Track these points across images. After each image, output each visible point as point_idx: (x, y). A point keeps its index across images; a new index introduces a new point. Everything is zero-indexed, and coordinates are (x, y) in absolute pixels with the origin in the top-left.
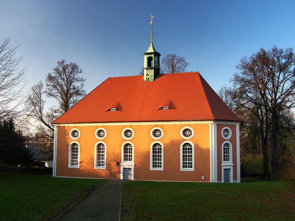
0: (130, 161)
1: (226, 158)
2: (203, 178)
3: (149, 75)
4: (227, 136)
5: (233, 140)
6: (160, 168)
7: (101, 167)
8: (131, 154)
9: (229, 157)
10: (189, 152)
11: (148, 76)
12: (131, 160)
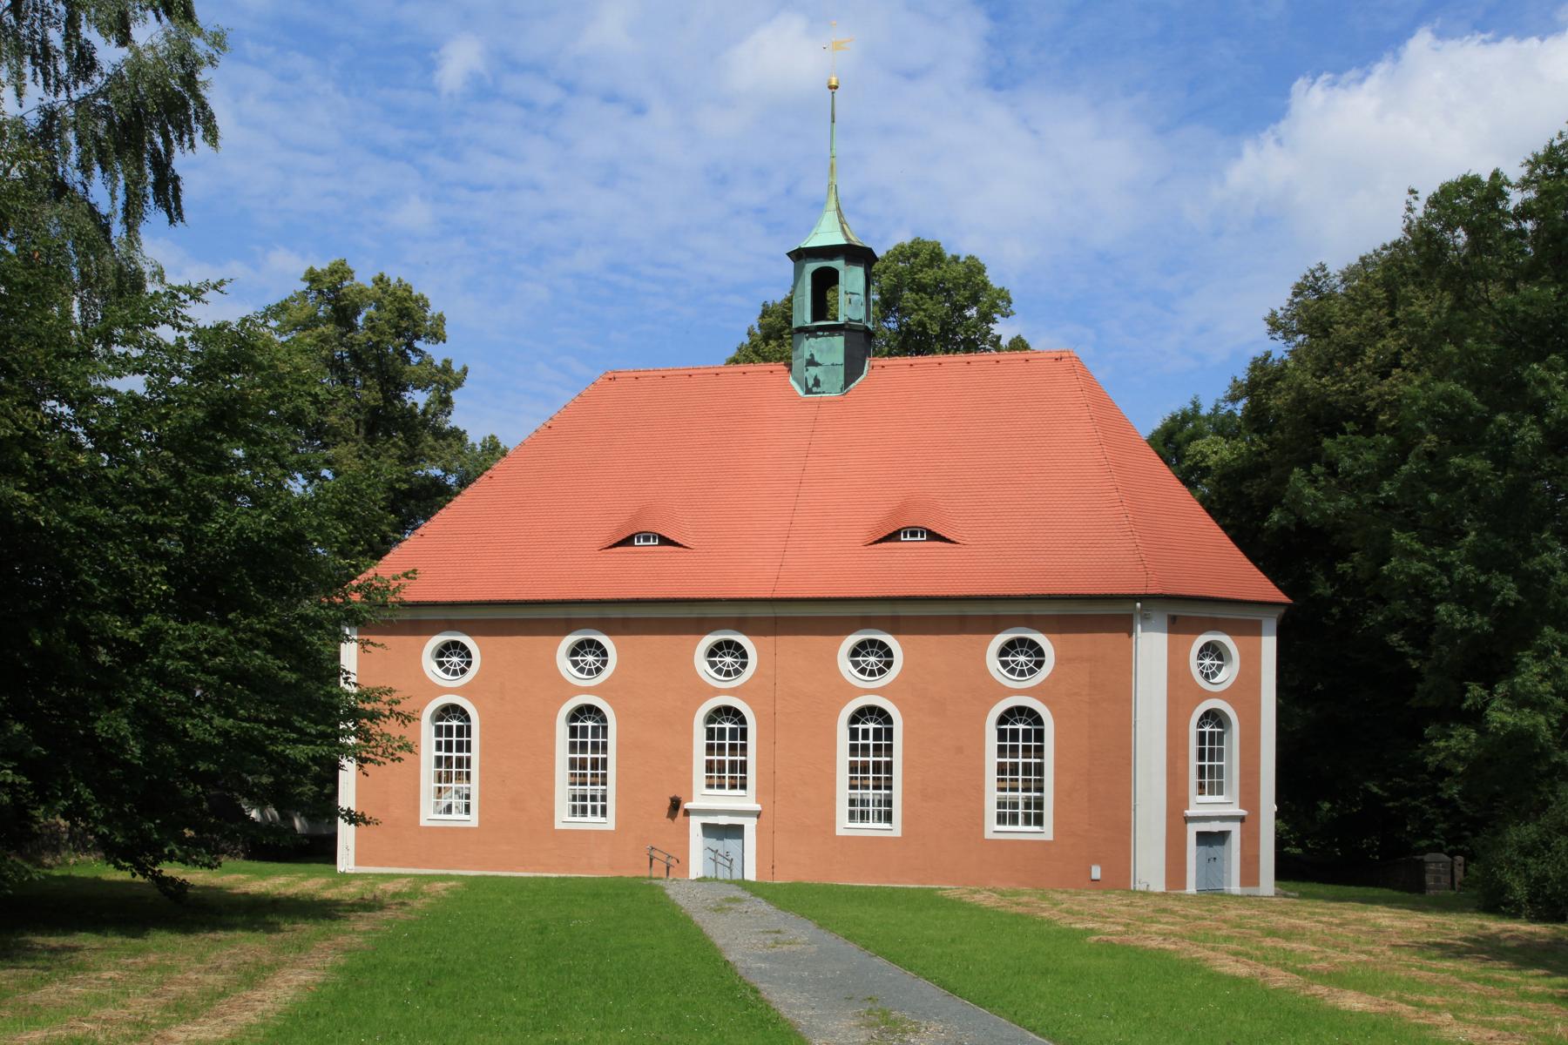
0: (738, 792)
1: (1210, 779)
2: (1096, 872)
3: (816, 364)
4: (1214, 675)
5: (1245, 691)
6: (1033, 828)
7: (591, 822)
8: (600, 756)
9: (1220, 775)
10: (1027, 749)
11: (813, 371)
12: (744, 787)
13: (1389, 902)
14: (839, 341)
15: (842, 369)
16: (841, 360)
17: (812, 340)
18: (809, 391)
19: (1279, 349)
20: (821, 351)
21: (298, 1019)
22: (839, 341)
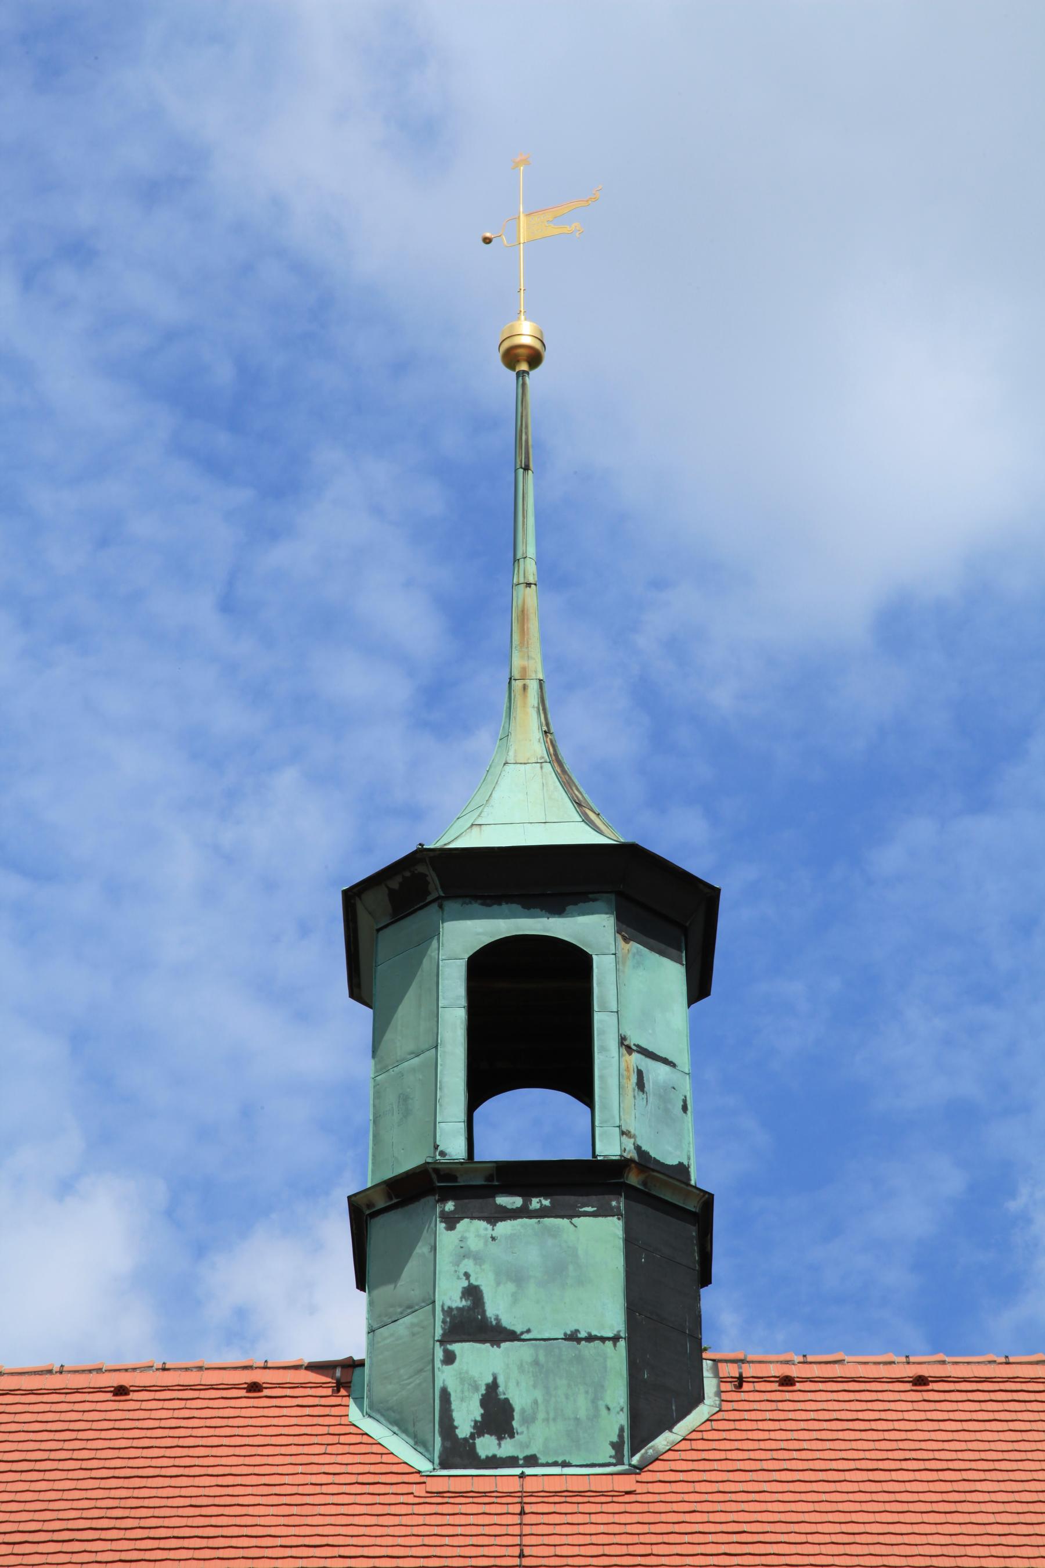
3: (496, 1334)
11: (477, 1361)
13: (584, 914)
14: (598, 1239)
15: (617, 1357)
16: (612, 1318)
17: (473, 1231)
18: (457, 1453)
19: (1013, 1206)
20: (517, 1277)
21: (536, 485)
22: (598, 1239)
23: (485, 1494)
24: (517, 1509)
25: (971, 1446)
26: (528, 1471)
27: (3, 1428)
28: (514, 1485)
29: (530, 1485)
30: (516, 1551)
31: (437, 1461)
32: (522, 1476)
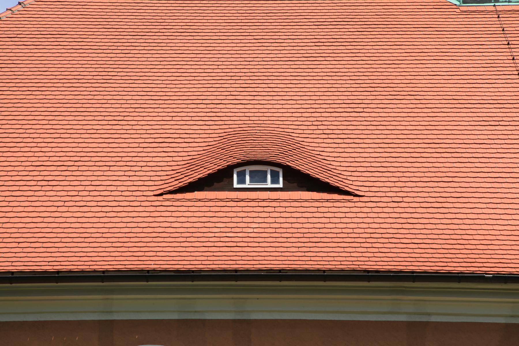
23: (483, 11)
24: (496, 16)
25: (468, 150)
26: (496, 4)
27: (1, 164)
28: (493, 9)
29: (499, 8)
30: (501, 29)
31: (461, 1)
32: (494, 6)
